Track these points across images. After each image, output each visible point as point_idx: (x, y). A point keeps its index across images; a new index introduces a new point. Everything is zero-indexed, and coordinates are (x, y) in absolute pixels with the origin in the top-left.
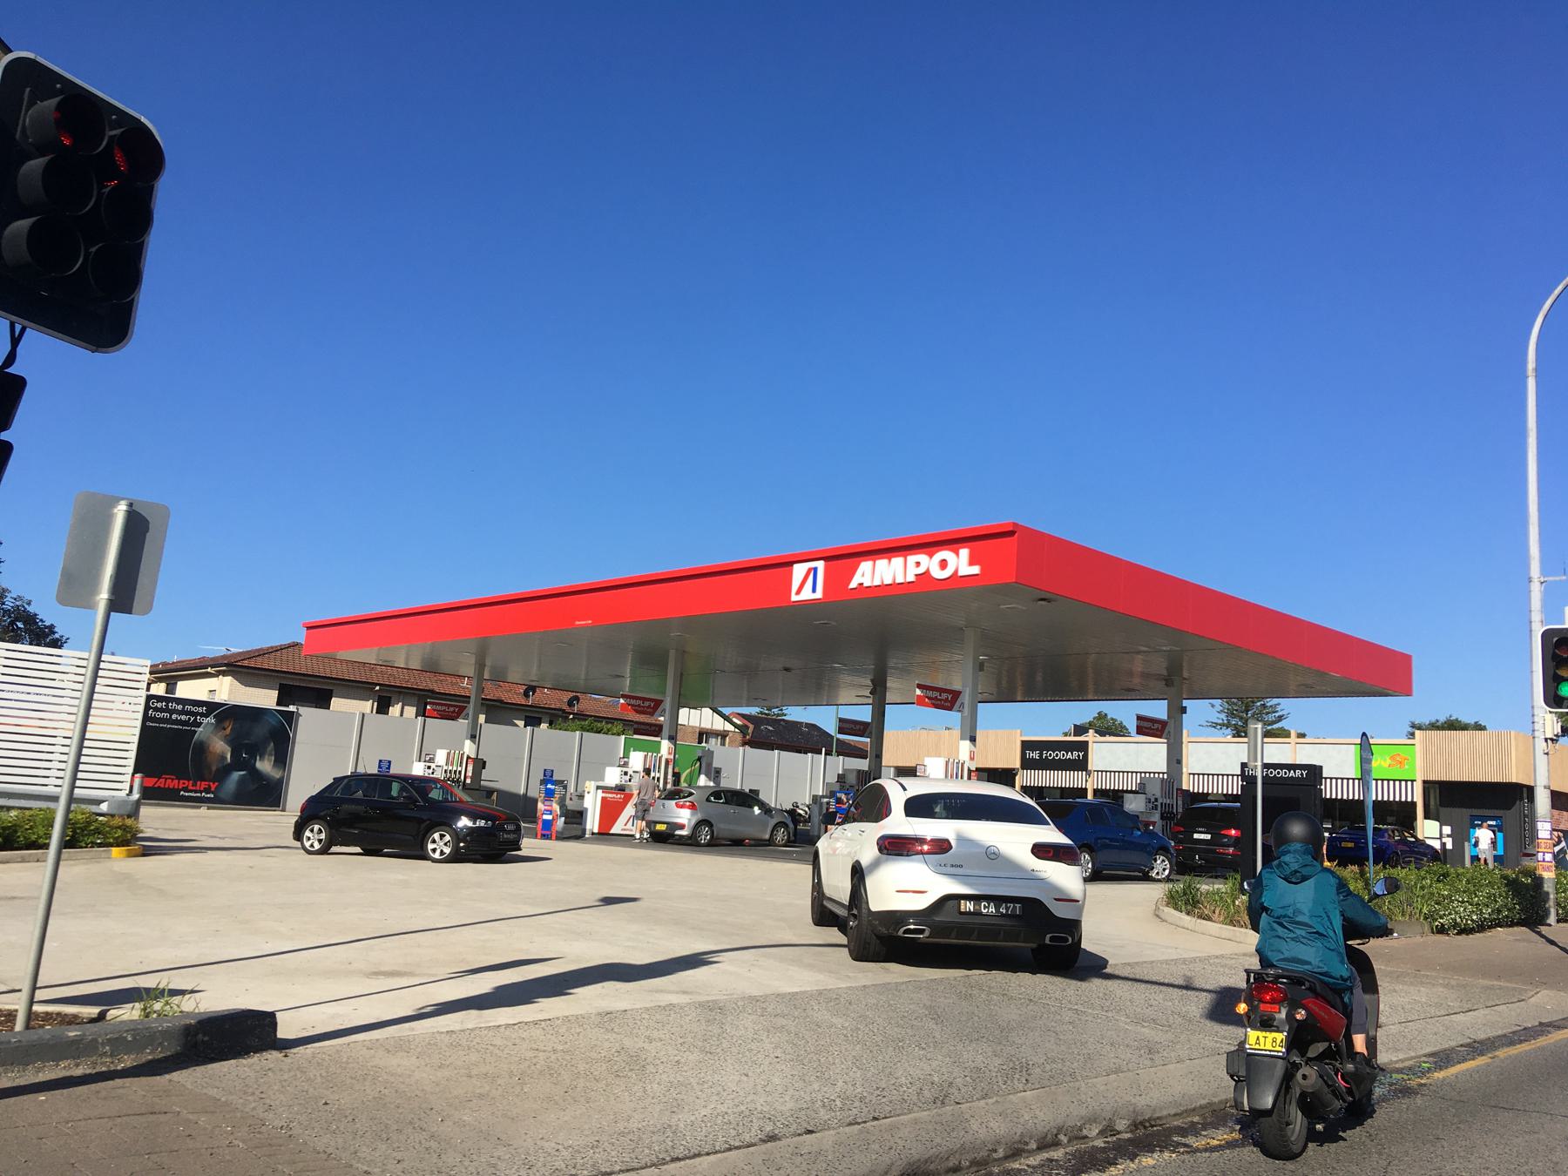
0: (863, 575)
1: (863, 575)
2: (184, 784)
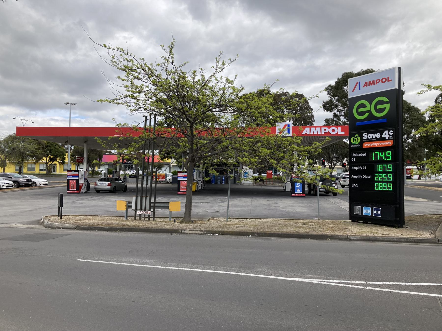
0: (307, 131)
1: (307, 131)
2: (325, 130)
